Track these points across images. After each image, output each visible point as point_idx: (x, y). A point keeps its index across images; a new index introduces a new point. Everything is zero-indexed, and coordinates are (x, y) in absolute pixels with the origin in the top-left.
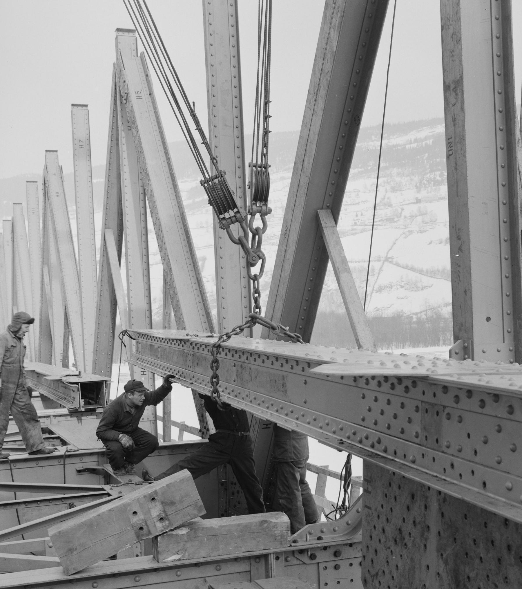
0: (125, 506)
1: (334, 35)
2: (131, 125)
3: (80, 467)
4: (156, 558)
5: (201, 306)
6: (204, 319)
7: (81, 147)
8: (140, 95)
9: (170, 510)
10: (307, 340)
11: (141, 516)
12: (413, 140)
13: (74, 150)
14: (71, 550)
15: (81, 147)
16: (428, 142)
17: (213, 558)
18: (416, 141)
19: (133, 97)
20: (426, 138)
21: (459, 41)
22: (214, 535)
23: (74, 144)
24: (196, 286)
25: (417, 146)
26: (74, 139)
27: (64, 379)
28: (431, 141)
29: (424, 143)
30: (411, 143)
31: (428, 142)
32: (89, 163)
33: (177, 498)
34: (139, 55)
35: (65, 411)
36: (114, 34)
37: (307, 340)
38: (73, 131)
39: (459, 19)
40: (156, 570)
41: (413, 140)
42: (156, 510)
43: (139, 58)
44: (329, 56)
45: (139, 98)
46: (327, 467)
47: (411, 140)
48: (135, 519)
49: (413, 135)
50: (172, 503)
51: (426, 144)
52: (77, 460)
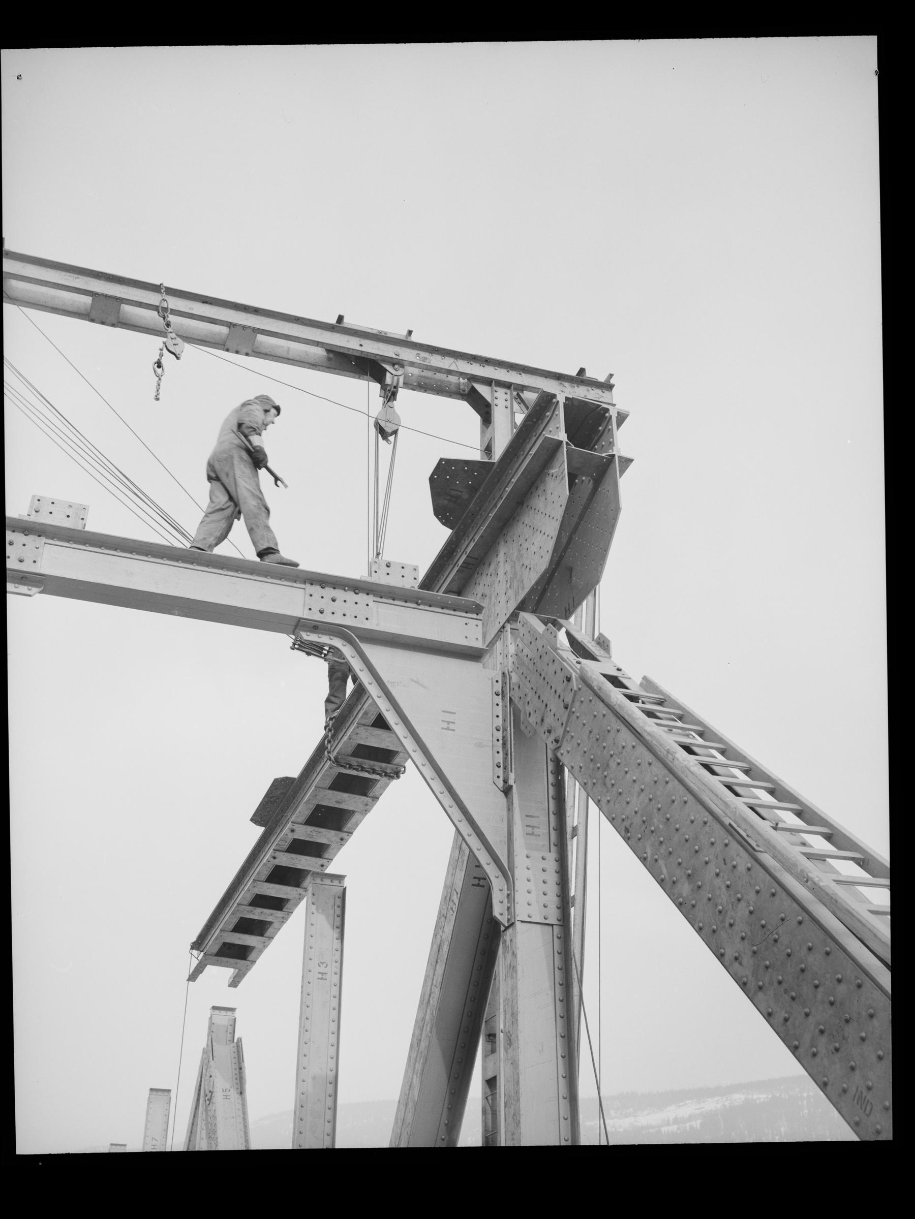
1: (416, 1081)
8: (228, 1093)
12: (671, 1119)
16: (693, 1123)
18: (676, 1121)
20: (691, 1118)
21: (518, 1124)
25: (679, 1129)
28: (699, 1122)
29: (688, 1125)
30: (668, 1124)
31: (693, 1123)
32: (337, 944)
34: (235, 1040)
36: (208, 1012)
38: (146, 1126)
39: (518, 1100)
41: (671, 1119)
43: (234, 1044)
44: (410, 1105)
47: (668, 1120)
49: (671, 1112)
51: (691, 1127)
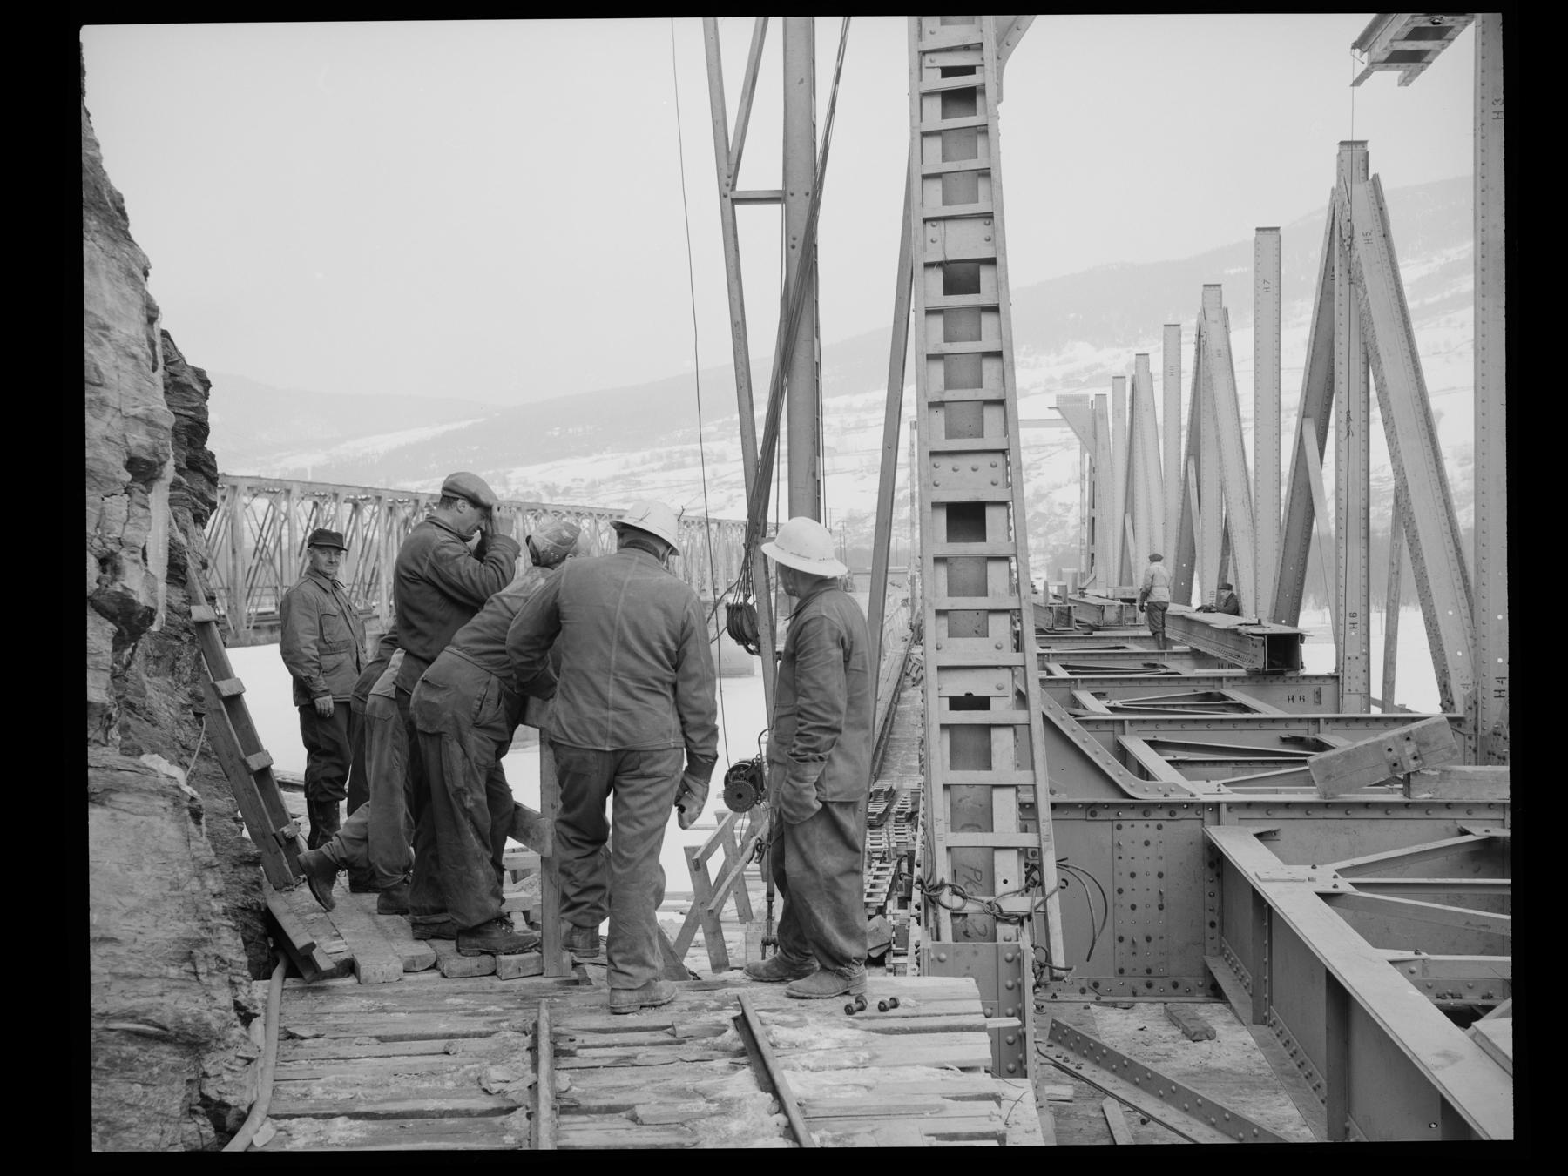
0: (1381, 742)
2: (1354, 280)
3: (1285, 734)
4: (1407, 794)
5: (1448, 538)
6: (1453, 556)
7: (1267, 290)
9: (1424, 750)
10: (980, 339)
11: (1395, 752)
13: (1257, 295)
14: (1329, 777)
15: (1267, 290)
17: (1466, 799)
19: (1359, 241)
22: (1467, 779)
23: (1257, 287)
24: (1442, 511)
26: (1257, 279)
27: (1242, 629)
33: (1432, 740)
35: (1241, 672)
37: (980, 339)
40: (1407, 805)
42: (1410, 749)
45: (1368, 242)
46: (1405, 82)
48: (1390, 755)
50: (1426, 744)
52: (1282, 726)
